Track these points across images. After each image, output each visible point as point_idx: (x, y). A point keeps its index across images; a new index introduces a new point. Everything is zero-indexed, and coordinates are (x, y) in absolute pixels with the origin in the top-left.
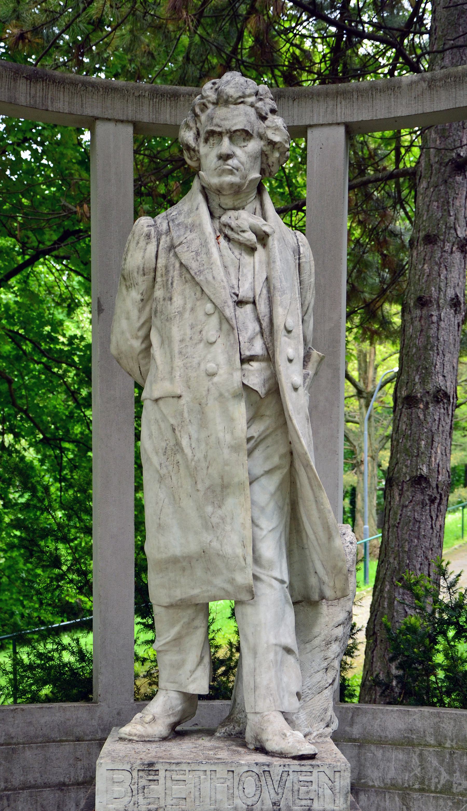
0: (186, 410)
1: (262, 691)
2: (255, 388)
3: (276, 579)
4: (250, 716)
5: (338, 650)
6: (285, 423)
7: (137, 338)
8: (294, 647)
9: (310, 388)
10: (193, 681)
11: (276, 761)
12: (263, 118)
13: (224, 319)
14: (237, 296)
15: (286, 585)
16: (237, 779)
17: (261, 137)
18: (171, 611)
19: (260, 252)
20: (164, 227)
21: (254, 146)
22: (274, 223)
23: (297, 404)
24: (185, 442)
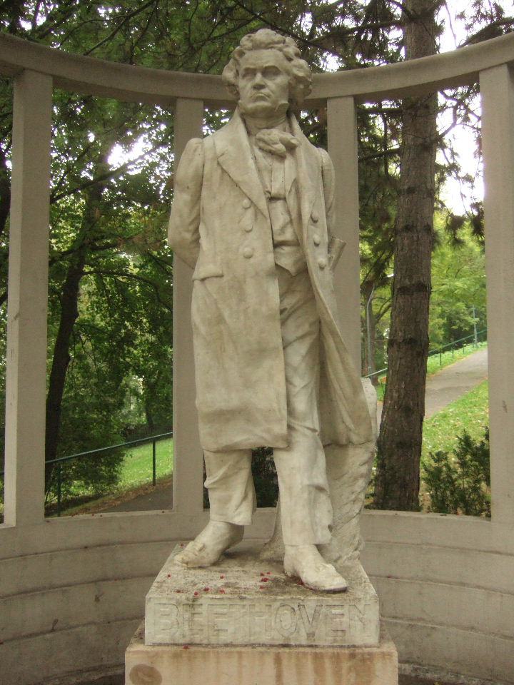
2: (287, 268)
3: (308, 428)
5: (364, 485)
7: (188, 231)
8: (327, 487)
9: (333, 268)
12: (290, 59)
13: (258, 212)
14: (270, 193)
15: (317, 433)
17: (288, 73)
18: (219, 455)
19: (289, 162)
21: (281, 80)
22: (298, 137)
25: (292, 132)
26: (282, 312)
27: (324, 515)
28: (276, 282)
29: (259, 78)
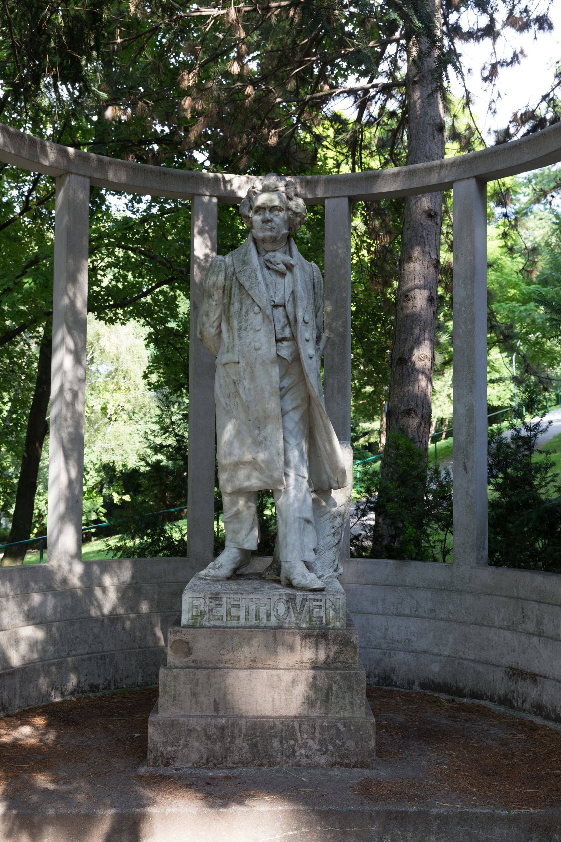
0: (242, 370)
1: (290, 547)
4: (283, 564)
6: (305, 379)
7: (213, 327)
8: (312, 520)
10: (248, 541)
11: (299, 593)
13: (266, 317)
16: (272, 604)
19: (289, 277)
22: (297, 258)
24: (241, 391)
25: (291, 255)
26: (281, 389)
27: (310, 541)
28: (277, 367)
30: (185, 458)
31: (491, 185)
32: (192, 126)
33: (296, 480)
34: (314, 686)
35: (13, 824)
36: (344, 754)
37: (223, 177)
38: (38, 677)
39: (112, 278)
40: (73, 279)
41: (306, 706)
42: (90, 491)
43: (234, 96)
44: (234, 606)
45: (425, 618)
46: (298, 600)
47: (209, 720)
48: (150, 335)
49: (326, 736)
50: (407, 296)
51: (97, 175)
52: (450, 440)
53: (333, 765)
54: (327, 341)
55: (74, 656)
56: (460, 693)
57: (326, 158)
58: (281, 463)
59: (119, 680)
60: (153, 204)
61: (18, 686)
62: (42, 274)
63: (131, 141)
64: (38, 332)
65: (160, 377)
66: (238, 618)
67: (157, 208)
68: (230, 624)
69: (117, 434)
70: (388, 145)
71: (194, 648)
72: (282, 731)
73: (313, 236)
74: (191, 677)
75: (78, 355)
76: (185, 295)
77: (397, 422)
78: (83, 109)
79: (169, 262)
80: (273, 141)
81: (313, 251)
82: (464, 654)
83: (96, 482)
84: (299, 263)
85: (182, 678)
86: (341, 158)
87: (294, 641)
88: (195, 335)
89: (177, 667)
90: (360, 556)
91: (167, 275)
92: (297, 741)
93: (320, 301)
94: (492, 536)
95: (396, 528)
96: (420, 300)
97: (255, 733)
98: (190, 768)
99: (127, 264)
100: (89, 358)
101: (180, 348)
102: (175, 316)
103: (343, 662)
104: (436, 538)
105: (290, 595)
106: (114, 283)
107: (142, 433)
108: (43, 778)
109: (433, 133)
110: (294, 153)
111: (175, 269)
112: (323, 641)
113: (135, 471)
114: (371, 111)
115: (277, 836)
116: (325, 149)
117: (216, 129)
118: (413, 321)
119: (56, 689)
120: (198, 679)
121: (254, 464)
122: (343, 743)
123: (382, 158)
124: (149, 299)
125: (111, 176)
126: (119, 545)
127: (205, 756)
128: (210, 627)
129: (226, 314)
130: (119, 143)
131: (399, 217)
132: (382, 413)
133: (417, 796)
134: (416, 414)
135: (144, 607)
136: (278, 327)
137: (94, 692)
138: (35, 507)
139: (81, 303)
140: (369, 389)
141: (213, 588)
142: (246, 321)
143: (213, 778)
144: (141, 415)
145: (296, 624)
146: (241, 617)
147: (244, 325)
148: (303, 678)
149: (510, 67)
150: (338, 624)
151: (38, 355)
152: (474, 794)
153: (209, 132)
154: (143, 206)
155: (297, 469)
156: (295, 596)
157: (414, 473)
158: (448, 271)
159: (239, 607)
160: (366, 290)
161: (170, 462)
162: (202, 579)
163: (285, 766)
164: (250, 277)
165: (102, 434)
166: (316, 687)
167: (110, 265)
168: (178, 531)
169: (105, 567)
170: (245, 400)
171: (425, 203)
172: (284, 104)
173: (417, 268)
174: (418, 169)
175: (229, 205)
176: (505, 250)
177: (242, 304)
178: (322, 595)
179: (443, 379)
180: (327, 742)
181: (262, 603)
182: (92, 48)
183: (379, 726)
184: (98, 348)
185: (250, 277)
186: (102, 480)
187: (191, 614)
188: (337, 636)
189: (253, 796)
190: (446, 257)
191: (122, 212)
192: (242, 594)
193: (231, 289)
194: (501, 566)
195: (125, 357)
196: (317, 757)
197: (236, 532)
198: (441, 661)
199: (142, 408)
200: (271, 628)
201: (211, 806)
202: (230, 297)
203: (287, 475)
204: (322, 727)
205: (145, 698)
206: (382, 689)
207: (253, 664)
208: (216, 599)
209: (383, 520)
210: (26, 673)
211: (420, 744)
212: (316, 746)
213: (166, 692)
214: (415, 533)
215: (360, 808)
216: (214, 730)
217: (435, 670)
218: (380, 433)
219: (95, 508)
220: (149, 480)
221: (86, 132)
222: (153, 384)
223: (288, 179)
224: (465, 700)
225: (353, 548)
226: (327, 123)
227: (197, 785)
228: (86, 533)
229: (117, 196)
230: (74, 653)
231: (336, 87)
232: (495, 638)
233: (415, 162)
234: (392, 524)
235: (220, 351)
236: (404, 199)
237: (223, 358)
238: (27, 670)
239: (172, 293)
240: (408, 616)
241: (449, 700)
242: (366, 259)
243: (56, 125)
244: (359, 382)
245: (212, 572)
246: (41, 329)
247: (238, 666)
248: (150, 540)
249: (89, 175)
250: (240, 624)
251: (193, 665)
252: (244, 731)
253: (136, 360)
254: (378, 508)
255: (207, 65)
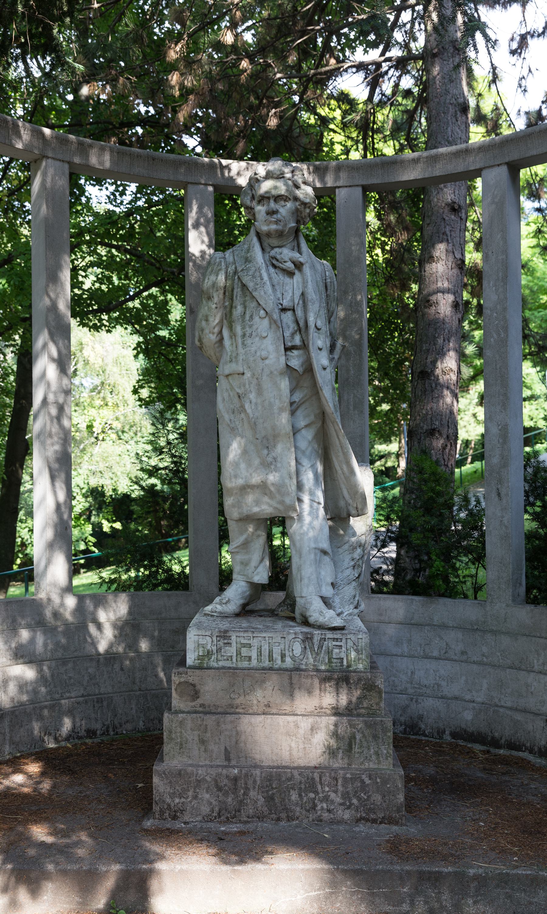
1: (306, 581)
4: (298, 599)
6: (318, 393)
7: (213, 333)
8: (329, 551)
10: (257, 574)
11: (316, 632)
13: (273, 322)
19: (298, 276)
20: (231, 259)
22: (306, 255)
23: (325, 378)
24: (247, 406)
26: (292, 404)
27: (327, 574)
28: (287, 379)
29: (272, 204)
30: (184, 482)
31: (524, 174)
32: (180, 106)
33: (311, 506)
34: (335, 734)
35: (9, 878)
36: (370, 808)
37: (220, 163)
38: (30, 721)
39: (95, 279)
40: (53, 277)
41: (326, 756)
42: (78, 518)
43: (227, 72)
44: (244, 645)
45: (455, 661)
46: (316, 639)
47: (220, 770)
48: (139, 344)
49: (350, 788)
50: (428, 301)
51: (77, 160)
52: (478, 465)
53: (358, 820)
54: (342, 350)
55: (68, 698)
56: (495, 743)
57: (332, 143)
58: (294, 487)
59: (118, 726)
60: (139, 195)
61: (7, 730)
62: (17, 275)
63: (111, 123)
64: (14, 340)
65: (151, 392)
66: (250, 658)
67: (144, 200)
68: (240, 665)
69: (105, 455)
70: (403, 128)
71: (202, 691)
72: (301, 783)
73: (320, 233)
74: (199, 722)
75: (63, 363)
76: (177, 300)
77: (419, 443)
78: (57, 86)
79: (158, 262)
80: (273, 122)
81: (323, 248)
82: (500, 700)
83: (83, 509)
84: (309, 261)
85: (189, 724)
86: (349, 143)
87: (312, 684)
88: (193, 343)
89: (183, 712)
90: (382, 592)
91: (155, 277)
92: (318, 793)
93: (334, 305)
94: (530, 571)
95: (421, 561)
96: (444, 305)
97: (271, 785)
98: (201, 821)
99: (109, 264)
100: (72, 369)
101: (173, 359)
102: (166, 323)
103: (367, 708)
104: (466, 572)
105: (307, 633)
106: (97, 285)
107: (133, 454)
108: (39, 830)
109: (456, 114)
110: (297, 137)
111: (167, 269)
112: (345, 685)
113: (126, 497)
114: (384, 89)
115: (299, 897)
116: (331, 133)
117: (207, 110)
118: (436, 329)
119: (50, 734)
120: (206, 725)
121: (263, 487)
122: (368, 797)
123: (397, 144)
124: (136, 303)
125: (94, 160)
126: (113, 577)
127: (217, 809)
128: (218, 669)
129: (228, 318)
130: (101, 124)
131: (416, 211)
132: (400, 434)
133: (452, 855)
134: (441, 434)
135: (144, 646)
136: (287, 334)
137: (91, 738)
138: (17, 535)
139: (63, 306)
140: (385, 407)
141: (220, 626)
142: (251, 326)
143: (226, 833)
144: (132, 434)
145: (314, 665)
146: (253, 658)
147: (248, 331)
148: (323, 725)
149: (541, 38)
150: (361, 666)
151: (15, 367)
152: (515, 854)
153: (200, 114)
154: (127, 198)
155: (312, 493)
156: (312, 635)
157: (441, 500)
158: (476, 273)
159: (250, 646)
160: (381, 294)
161: (165, 486)
162: (208, 615)
163: (305, 821)
164: (254, 276)
165: (89, 455)
166: (337, 735)
167: (92, 264)
168: (179, 562)
169: (99, 601)
170: (251, 416)
171: (449, 194)
172: (285, 80)
173: (440, 268)
174: (442, 154)
175: (227, 195)
176: (538, 250)
177: (245, 307)
178: (343, 634)
179: (468, 396)
180: (351, 796)
181: (278, 642)
182: (65, 14)
183: (408, 779)
184: (81, 360)
185: (254, 276)
186: (90, 506)
187: (196, 654)
188: (359, 680)
189: (271, 853)
190: (473, 257)
191: (103, 204)
192: (253, 632)
193: (233, 290)
194: (539, 604)
195: (112, 369)
196: (340, 811)
197: (245, 564)
198: (474, 708)
199: (131, 426)
200: (286, 670)
201: (226, 862)
202: (232, 299)
203: (300, 500)
204: (345, 779)
205: (150, 745)
206: (409, 738)
207: (267, 710)
208: (225, 637)
209: (407, 552)
210: (16, 716)
211: (454, 799)
212: (338, 799)
213: (172, 739)
214: (443, 567)
215: (390, 867)
216: (226, 781)
217: (467, 717)
218: (398, 456)
219: (84, 537)
220: (142, 507)
221: (60, 113)
222: (144, 400)
223: (294, 164)
224: (502, 752)
225: (373, 583)
226: (333, 103)
227: (208, 841)
228: (74, 565)
229: (97, 187)
230: (68, 695)
231: (343, 61)
232: (535, 684)
233: (436, 147)
234: (416, 557)
235: (222, 361)
236: (423, 190)
237: (225, 369)
238: (17, 713)
239: (162, 298)
240: (436, 658)
241: (484, 751)
242: (381, 260)
243: (26, 105)
244: (374, 399)
245: (219, 608)
246: (17, 337)
247: (251, 711)
248: (147, 573)
249: (68, 160)
250: (252, 666)
251: (201, 709)
252: (258, 783)
253: (124, 372)
254: (399, 538)
255: (196, 35)
